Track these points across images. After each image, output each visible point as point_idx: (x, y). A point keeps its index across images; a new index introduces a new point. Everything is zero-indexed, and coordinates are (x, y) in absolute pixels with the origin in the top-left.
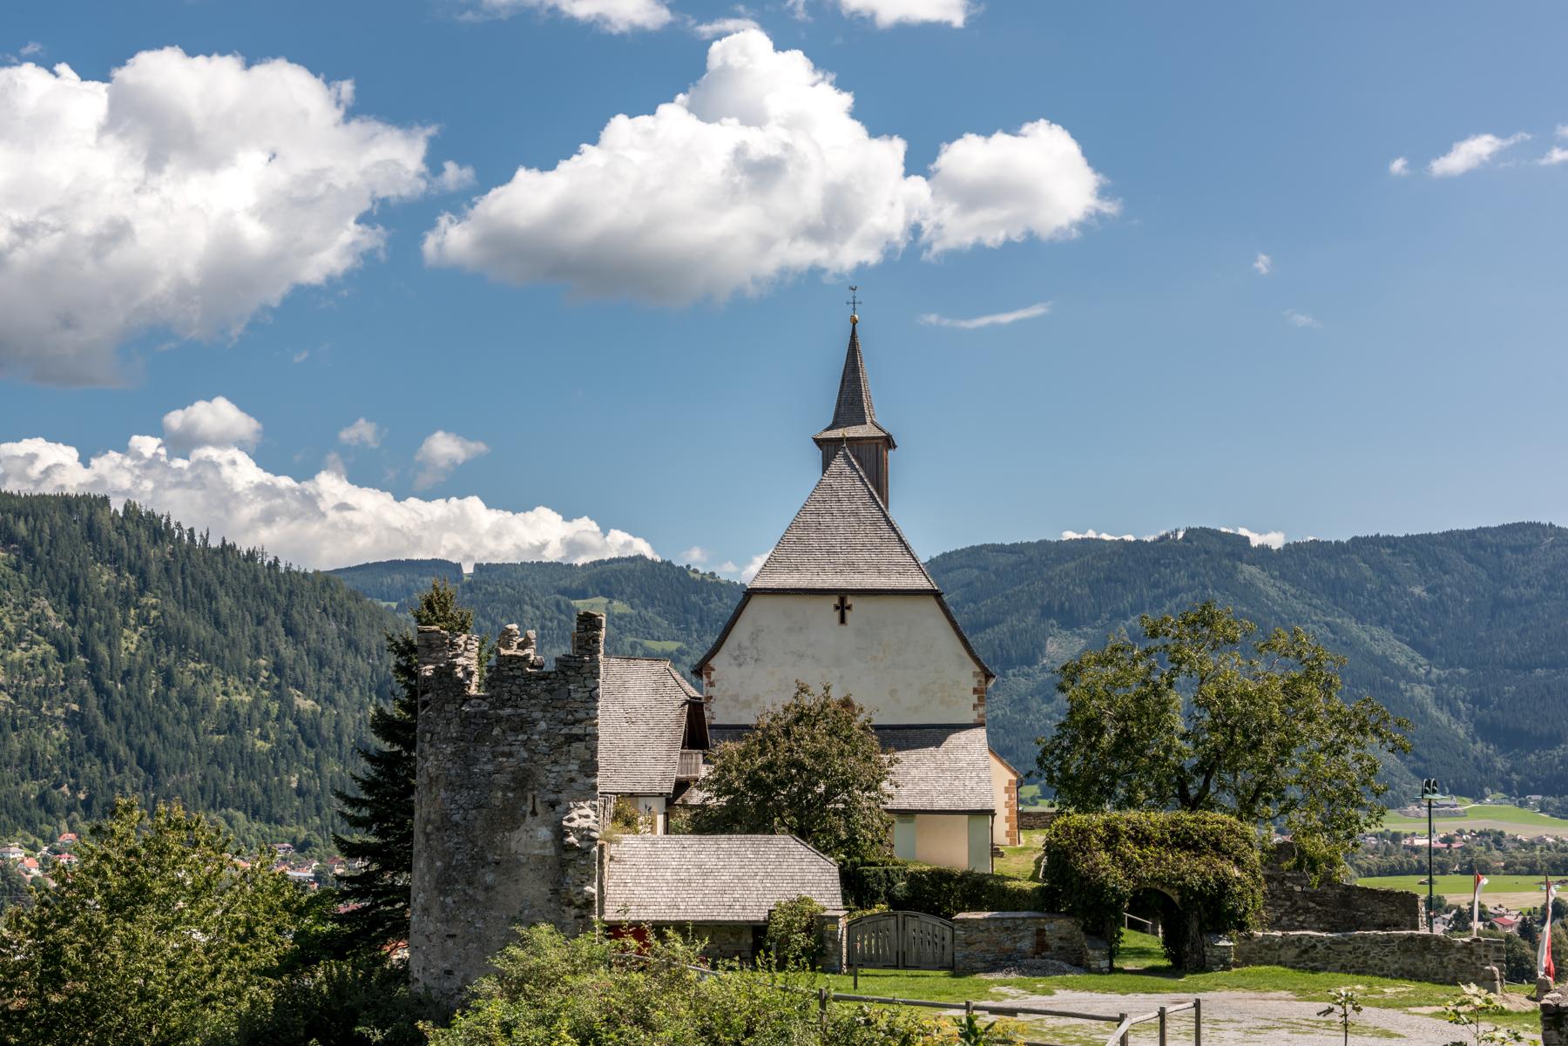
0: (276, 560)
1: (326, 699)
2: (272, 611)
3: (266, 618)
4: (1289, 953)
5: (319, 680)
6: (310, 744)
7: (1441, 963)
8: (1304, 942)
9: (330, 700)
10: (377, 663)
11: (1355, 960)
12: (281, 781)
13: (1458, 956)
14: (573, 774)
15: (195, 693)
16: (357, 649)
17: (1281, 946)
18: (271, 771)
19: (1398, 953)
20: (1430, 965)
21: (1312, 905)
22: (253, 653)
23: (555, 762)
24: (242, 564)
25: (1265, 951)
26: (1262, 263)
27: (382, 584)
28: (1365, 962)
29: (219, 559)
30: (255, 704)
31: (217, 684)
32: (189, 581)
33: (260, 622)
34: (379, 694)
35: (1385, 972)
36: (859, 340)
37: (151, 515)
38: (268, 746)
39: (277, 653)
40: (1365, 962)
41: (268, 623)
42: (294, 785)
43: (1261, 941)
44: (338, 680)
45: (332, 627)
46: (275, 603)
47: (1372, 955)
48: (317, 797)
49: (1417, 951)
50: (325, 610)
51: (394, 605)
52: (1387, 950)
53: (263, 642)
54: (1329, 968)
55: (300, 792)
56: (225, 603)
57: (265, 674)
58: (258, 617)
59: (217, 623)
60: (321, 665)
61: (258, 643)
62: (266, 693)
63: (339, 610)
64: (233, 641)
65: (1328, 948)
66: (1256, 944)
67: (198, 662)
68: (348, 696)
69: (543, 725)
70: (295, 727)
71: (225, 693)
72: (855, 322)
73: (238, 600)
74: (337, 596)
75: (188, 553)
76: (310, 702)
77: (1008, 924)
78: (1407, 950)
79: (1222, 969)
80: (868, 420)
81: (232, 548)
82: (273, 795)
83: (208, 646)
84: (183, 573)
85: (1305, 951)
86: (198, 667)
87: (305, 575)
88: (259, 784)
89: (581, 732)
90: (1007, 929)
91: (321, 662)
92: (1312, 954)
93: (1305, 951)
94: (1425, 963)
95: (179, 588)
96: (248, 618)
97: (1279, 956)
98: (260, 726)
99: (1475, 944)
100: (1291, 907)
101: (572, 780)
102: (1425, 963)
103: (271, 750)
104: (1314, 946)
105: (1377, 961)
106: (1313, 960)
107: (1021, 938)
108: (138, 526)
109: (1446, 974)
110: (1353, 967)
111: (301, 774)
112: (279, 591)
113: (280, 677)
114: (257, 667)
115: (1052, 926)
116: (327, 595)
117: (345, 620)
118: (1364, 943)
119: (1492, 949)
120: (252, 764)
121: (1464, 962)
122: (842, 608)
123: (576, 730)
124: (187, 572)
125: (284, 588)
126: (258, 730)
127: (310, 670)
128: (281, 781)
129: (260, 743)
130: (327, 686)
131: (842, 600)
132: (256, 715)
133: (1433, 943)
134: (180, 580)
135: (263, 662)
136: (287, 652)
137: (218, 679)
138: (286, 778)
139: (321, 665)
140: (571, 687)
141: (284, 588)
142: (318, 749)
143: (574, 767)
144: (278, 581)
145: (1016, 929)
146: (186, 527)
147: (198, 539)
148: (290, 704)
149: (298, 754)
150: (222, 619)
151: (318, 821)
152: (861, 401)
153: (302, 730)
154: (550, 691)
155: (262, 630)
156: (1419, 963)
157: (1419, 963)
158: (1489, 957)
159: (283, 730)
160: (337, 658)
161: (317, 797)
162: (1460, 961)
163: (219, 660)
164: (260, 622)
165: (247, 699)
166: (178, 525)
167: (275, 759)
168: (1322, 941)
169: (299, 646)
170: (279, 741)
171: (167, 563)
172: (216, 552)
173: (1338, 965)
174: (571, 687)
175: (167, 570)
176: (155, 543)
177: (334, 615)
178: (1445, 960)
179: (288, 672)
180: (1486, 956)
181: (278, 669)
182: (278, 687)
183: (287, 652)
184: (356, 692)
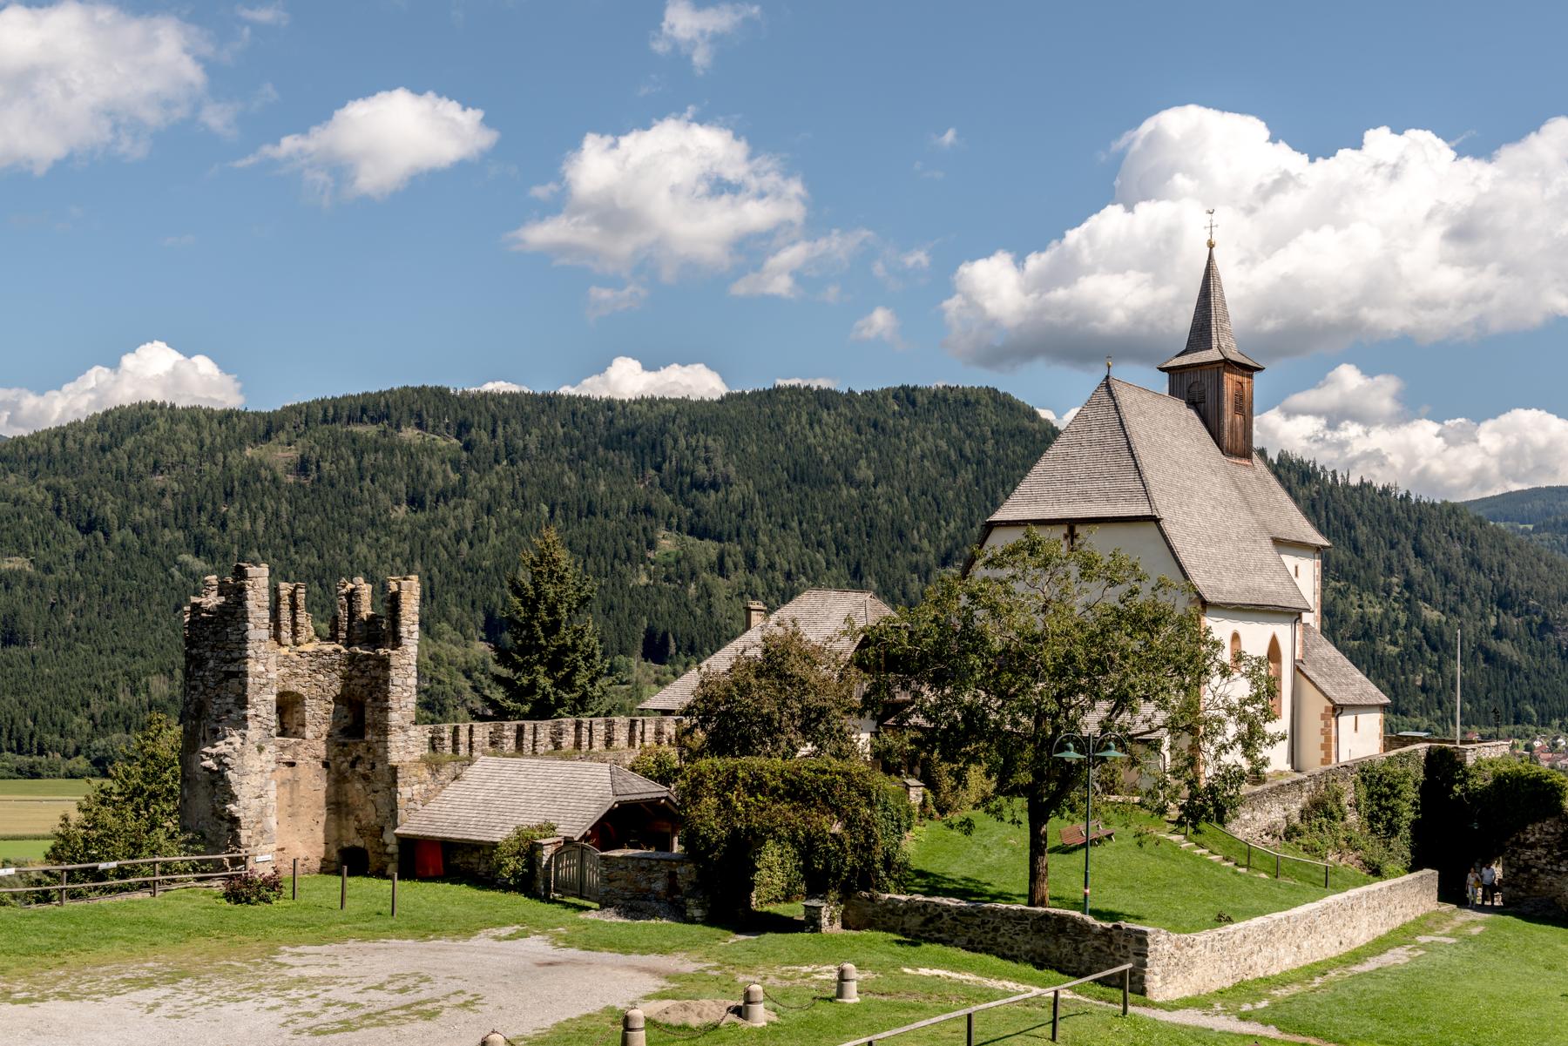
0: (1408, 493)
1: (1451, 610)
2: (1403, 537)
3: (1398, 543)
4: (914, 920)
5: (1444, 594)
6: (1434, 649)
7: (1076, 949)
8: (929, 910)
9: (1454, 610)
10: (1498, 578)
11: (984, 935)
12: (1407, 680)
13: (1096, 943)
15: (1335, 606)
16: (1480, 567)
17: (905, 912)
18: (1398, 670)
19: (1030, 933)
20: (1065, 951)
22: (1387, 572)
23: (218, 696)
24: (1378, 499)
25: (888, 915)
26: (950, 136)
27: (1523, 509)
28: (994, 939)
29: (1357, 495)
30: (1385, 615)
31: (1354, 599)
32: (1331, 515)
33: (1393, 547)
34: (1499, 605)
35: (1015, 952)
37: (1301, 462)
38: (1397, 650)
39: (1407, 572)
40: (994, 939)
41: (1400, 547)
42: (1419, 683)
43: (886, 904)
44: (1462, 594)
45: (1457, 549)
46: (1406, 530)
47: (1002, 931)
48: (1439, 694)
49: (1051, 933)
50: (1451, 534)
51: (1531, 527)
52: (1018, 928)
53: (1395, 563)
54: (956, 941)
55: (1424, 689)
56: (1362, 532)
57: (1397, 589)
58: (1391, 542)
59: (1356, 548)
60: (1447, 582)
61: (1391, 564)
62: (1396, 605)
63: (1463, 534)
64: (1369, 564)
65: (954, 919)
66: (880, 906)
67: (1338, 581)
68: (1470, 607)
69: (211, 664)
70: (1421, 635)
71: (1360, 606)
72: (1211, 246)
73: (1374, 529)
74: (1462, 522)
75: (1331, 491)
76: (1436, 613)
77: (644, 864)
78: (1040, 930)
79: (812, 931)
80: (1215, 344)
82: (1400, 690)
83: (1347, 568)
84: (1326, 507)
85: (930, 920)
86: (1338, 585)
87: (1433, 505)
88: (1388, 682)
90: (643, 869)
91: (1448, 578)
92: (938, 924)
93: (930, 920)
94: (1058, 948)
95: (1323, 521)
96: (1382, 543)
97: (903, 923)
98: (1390, 634)
99: (1115, 932)
101: (229, 711)
102: (1058, 948)
103: (1400, 655)
104: (940, 916)
105: (1005, 939)
106: (939, 931)
107: (656, 879)
108: (438, 500)
109: (1080, 962)
110: (981, 942)
111: (1424, 673)
112: (1410, 520)
113: (1411, 593)
114: (1390, 584)
115: (683, 870)
116: (1452, 521)
117: (1469, 541)
118: (995, 917)
119: (1133, 939)
120: (1382, 665)
121: (1102, 951)
122: (1072, 535)
123: (233, 668)
124: (1330, 507)
125: (1414, 517)
126: (1388, 637)
127: (1436, 586)
128: (1407, 680)
129: (1390, 648)
130: (1451, 599)
131: (1071, 530)
132: (1386, 625)
133: (1069, 925)
134: (1324, 513)
135: (1395, 580)
136: (1417, 571)
137: (1354, 594)
138: (1411, 676)
139: (1447, 582)
141: (1414, 517)
142: (1441, 652)
143: (231, 700)
144: (1408, 511)
145: (650, 869)
146: (1329, 470)
147: (1339, 479)
148: (1418, 615)
149: (1422, 656)
150: (1360, 545)
151: (1439, 713)
152: (1209, 326)
153: (1427, 638)
154: (215, 633)
155: (1394, 553)
156: (1052, 947)
157: (1052, 947)
158: (1129, 949)
159: (1410, 636)
160: (1461, 575)
161: (1439, 694)
162: (1097, 949)
163: (1355, 580)
164: (1393, 547)
165: (1379, 611)
166: (1323, 468)
167: (1402, 661)
168: (948, 911)
169: (1428, 566)
170: (1406, 647)
171: (1313, 500)
172: (1355, 489)
173: (964, 940)
175: (1313, 506)
176: (1304, 483)
177: (1459, 538)
178: (1081, 946)
179: (1417, 587)
180: (1125, 947)
181: (1408, 585)
182: (1408, 600)
183: (1417, 571)
184: (1478, 604)
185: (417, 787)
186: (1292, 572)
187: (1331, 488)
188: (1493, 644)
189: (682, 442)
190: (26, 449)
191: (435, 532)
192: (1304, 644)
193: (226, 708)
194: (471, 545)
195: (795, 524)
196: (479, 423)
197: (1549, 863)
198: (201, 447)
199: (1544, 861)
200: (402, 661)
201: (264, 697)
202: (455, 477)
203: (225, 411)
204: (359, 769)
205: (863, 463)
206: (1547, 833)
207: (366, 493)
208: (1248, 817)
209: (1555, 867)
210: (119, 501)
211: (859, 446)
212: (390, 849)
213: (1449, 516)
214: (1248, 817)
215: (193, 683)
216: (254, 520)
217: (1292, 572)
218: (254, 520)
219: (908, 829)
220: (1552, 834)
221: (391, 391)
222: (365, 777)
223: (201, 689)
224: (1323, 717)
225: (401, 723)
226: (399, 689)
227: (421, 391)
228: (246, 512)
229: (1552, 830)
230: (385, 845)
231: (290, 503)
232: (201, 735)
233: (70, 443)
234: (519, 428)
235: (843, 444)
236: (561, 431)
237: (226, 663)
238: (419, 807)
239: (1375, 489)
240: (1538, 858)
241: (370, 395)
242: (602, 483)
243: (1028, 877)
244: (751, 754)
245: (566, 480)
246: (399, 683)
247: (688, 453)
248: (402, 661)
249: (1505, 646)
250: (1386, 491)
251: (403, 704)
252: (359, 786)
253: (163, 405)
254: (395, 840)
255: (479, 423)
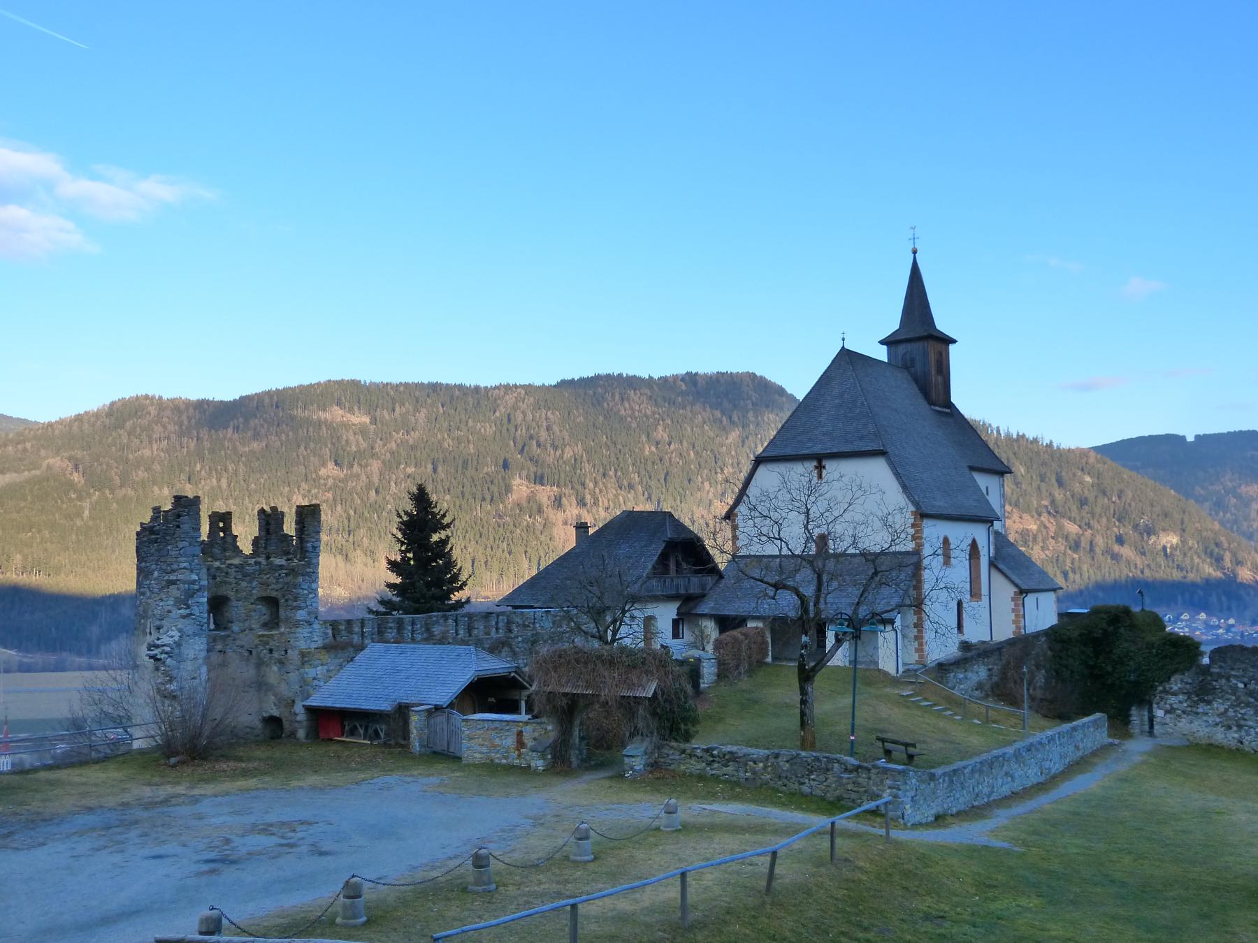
0: (1051, 442)
14: (170, 608)
21: (1252, 700)
36: (918, 261)
41: (1047, 480)
69: (156, 573)
72: (915, 252)
81: (1023, 436)
89: (175, 578)
100: (1235, 701)
101: (169, 612)
123: (172, 577)
127: (1074, 508)
130: (1087, 517)
136: (1059, 495)
140: (169, 548)
146: (994, 426)
174: (169, 548)
184: (1104, 520)
185: (320, 668)
186: (985, 492)
187: (997, 439)
188: (1116, 548)
189: (530, 416)
190: (53, 431)
191: (350, 485)
192: (996, 545)
193: (167, 608)
194: (377, 492)
195: (612, 473)
196: (383, 405)
197: (1188, 706)
198: (181, 426)
199: (1185, 705)
200: (308, 570)
201: (198, 600)
202: (364, 445)
203: (198, 401)
204: (276, 655)
205: (660, 428)
206: (1187, 683)
207: (301, 457)
208: (961, 676)
209: (1194, 709)
210: (121, 467)
211: (657, 416)
212: (298, 718)
213: (1081, 458)
214: (961, 676)
215: (142, 590)
216: (219, 480)
217: (985, 492)
218: (219, 480)
219: (967, 752)
220: (1190, 684)
221: (319, 384)
222: (281, 662)
223: (148, 594)
224: (1013, 599)
225: (307, 618)
226: (306, 592)
227: (340, 383)
228: (214, 472)
229: (1190, 681)
230: (296, 714)
231: (245, 465)
232: (148, 631)
233: (86, 426)
234: (411, 409)
235: (646, 416)
236: (441, 410)
237: (167, 573)
238: (322, 684)
239: (1027, 440)
240: (1180, 702)
241: (304, 386)
242: (471, 446)
243: (799, 724)
244: (925, 912)
245: (446, 445)
246: (306, 587)
247: (534, 424)
248: (308, 570)
249: (1126, 551)
250: (1035, 441)
251: (309, 603)
252: (275, 668)
253: (153, 397)
254: (303, 711)
255: (383, 405)
